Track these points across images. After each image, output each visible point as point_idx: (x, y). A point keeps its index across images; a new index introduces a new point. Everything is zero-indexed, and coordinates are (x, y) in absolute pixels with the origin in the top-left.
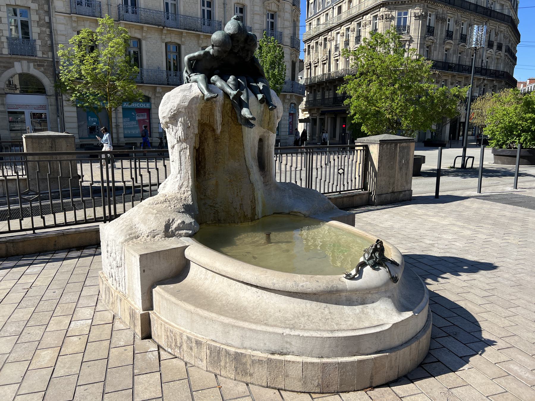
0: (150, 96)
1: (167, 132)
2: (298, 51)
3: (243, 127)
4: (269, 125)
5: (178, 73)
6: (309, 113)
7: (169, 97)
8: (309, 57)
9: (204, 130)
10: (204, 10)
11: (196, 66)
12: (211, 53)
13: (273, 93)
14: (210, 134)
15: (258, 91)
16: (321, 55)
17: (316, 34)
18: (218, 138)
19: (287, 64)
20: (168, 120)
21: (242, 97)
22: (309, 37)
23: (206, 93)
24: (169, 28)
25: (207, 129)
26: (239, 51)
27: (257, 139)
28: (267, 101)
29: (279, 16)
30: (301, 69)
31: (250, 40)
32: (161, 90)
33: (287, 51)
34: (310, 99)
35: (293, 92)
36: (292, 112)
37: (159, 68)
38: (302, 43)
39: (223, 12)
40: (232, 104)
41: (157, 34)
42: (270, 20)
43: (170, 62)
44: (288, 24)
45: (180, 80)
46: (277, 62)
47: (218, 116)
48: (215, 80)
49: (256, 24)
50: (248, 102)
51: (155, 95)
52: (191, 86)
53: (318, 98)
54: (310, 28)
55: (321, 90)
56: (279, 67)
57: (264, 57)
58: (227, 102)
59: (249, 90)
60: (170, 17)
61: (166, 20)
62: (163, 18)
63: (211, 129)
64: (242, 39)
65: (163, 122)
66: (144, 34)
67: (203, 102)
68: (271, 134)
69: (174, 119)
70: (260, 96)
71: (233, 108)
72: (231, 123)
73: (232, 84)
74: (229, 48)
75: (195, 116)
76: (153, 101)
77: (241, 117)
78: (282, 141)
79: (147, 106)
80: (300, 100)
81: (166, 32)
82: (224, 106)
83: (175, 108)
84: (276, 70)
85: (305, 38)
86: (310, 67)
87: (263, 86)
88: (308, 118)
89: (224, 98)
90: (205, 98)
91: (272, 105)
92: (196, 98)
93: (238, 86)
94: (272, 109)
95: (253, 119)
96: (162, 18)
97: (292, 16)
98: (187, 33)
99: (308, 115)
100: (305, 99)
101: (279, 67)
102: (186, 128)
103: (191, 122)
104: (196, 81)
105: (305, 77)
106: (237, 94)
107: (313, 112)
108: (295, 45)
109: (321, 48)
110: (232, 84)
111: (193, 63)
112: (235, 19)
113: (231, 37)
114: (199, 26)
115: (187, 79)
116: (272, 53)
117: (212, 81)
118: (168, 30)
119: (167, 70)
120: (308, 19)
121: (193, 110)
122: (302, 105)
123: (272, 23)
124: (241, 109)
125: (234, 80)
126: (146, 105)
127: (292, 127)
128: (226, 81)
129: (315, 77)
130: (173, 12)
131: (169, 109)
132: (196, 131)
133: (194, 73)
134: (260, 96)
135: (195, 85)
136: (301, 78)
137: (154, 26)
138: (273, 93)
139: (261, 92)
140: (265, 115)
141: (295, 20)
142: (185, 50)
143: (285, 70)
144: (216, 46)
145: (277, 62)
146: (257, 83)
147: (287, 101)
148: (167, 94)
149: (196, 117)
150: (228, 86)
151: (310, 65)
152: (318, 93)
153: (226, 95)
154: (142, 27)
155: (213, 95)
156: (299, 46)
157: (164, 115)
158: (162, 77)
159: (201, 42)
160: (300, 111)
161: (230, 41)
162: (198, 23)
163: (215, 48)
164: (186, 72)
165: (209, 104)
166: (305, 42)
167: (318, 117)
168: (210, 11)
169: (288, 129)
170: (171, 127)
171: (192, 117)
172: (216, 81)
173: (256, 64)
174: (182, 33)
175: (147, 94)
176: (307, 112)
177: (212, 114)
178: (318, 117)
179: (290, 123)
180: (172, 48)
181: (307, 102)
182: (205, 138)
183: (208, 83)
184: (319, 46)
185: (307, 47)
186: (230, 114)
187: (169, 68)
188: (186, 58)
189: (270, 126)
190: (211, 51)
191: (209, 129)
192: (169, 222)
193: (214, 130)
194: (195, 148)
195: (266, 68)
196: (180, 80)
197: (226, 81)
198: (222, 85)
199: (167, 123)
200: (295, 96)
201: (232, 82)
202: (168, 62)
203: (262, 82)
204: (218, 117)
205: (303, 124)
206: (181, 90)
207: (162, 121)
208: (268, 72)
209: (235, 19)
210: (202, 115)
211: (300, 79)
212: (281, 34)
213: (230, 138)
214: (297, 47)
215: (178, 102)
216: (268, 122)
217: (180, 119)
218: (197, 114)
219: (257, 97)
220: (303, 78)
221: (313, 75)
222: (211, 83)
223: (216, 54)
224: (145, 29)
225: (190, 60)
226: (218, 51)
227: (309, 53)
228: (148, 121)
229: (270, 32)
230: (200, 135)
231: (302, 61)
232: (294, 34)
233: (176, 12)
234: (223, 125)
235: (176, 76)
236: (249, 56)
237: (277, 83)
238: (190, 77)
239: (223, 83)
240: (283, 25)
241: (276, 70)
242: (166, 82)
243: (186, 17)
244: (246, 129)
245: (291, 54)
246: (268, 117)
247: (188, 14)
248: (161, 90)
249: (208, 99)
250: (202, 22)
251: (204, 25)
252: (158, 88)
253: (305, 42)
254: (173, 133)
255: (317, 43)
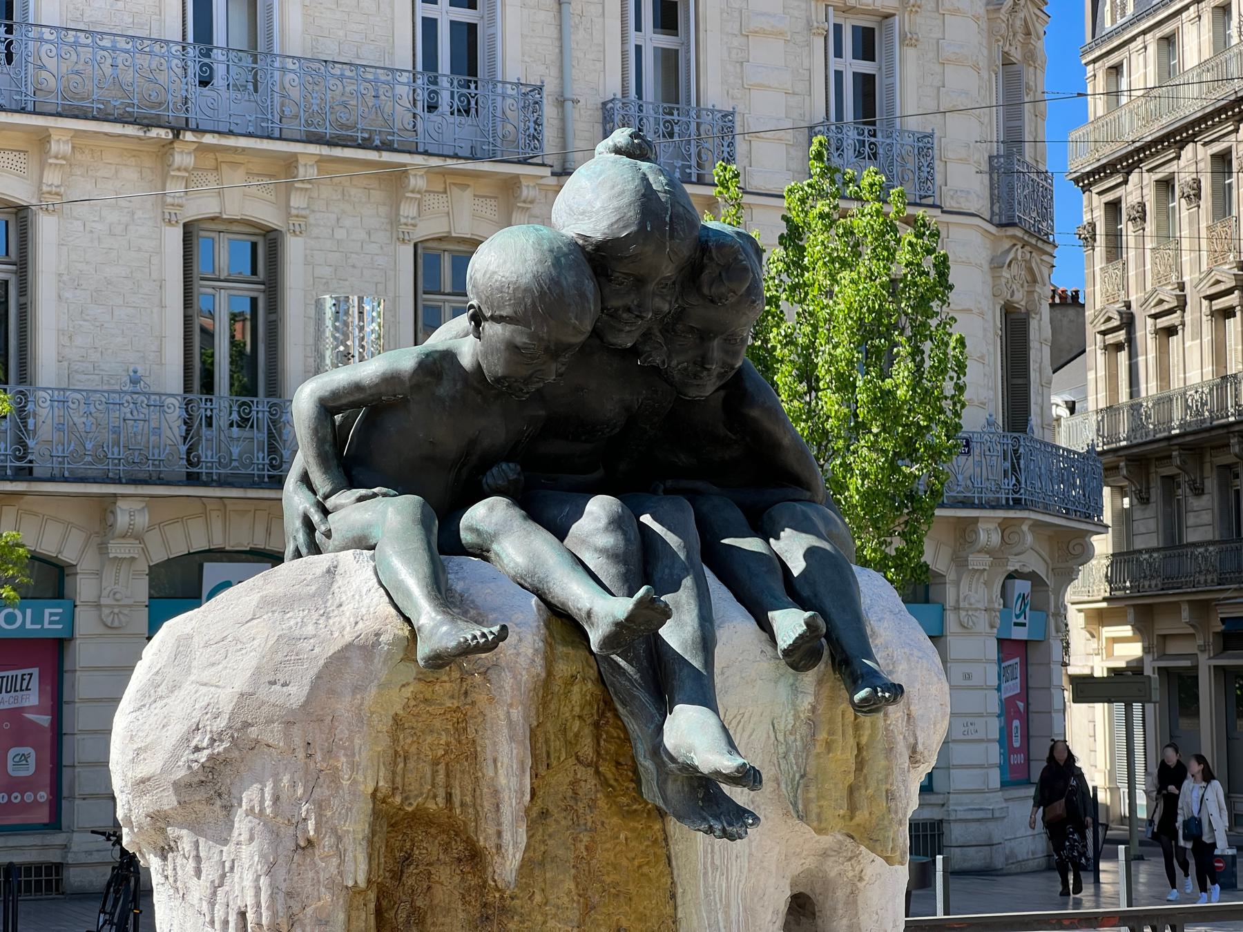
0: (68, 556)
1: (156, 879)
2: (1039, 239)
3: (675, 827)
4: (853, 809)
5: (260, 407)
6: (1143, 629)
7: (182, 649)
8: (1115, 270)
9: (408, 859)
10: (430, 26)
11: (363, 443)
12: (466, 360)
13: (876, 593)
14: (447, 882)
15: (779, 587)
16: (1198, 260)
17: (1151, 132)
18: (503, 910)
19: (971, 318)
20: (169, 801)
21: (664, 632)
22: (1108, 152)
23: (426, 614)
24: (209, 139)
25: (429, 848)
26: (647, 335)
27: (779, 899)
28: (836, 651)
29: (908, 40)
30: (1069, 352)
31: (717, 269)
32: (142, 520)
33: (969, 248)
34: (1139, 544)
35: (1018, 504)
36: (1019, 634)
37: (135, 381)
38: (1063, 190)
39: (552, 31)
40: (601, 680)
41: (130, 174)
42: (851, 66)
43: (208, 334)
44: (972, 84)
45: (273, 450)
46: (905, 314)
47: (504, 760)
48: (485, 527)
49: (759, 195)
50: (709, 661)
51: (103, 549)
52: (331, 572)
53: (1191, 537)
54: (1114, 94)
55: (1211, 484)
56: (916, 352)
57: (806, 338)
58: (563, 669)
59: (708, 572)
60: (220, 70)
61: (196, 91)
62: (171, 79)
63: (458, 848)
64: (668, 270)
65: (138, 815)
66: (52, 178)
67: (408, 673)
68: (873, 865)
69: (209, 787)
70: (790, 623)
71: (608, 703)
72: (592, 805)
73: (603, 551)
74: (579, 327)
75: (354, 767)
76: (84, 588)
77: (660, 766)
78: (955, 833)
79: (49, 620)
80: (1071, 553)
81: (189, 161)
82: (545, 692)
83: (222, 723)
84: (901, 373)
85: (1084, 162)
86: (1131, 340)
87: (810, 554)
88: (1135, 669)
89: (549, 643)
90: (423, 650)
91: (872, 677)
92: (365, 649)
93: (642, 564)
94: (869, 707)
95: (748, 777)
96: (171, 79)
97: (991, 32)
98: (322, 160)
99: (1135, 650)
100: (1103, 545)
101: (916, 352)
102: (293, 848)
103: (320, 807)
104: (363, 543)
105: (1096, 398)
106: (631, 617)
107: (1165, 626)
108: (1019, 206)
109: (1191, 221)
110: (603, 551)
111: (346, 424)
112: (618, 151)
113: (598, 259)
114: (402, 116)
115: (309, 526)
116: (865, 263)
117: (466, 537)
118: (202, 149)
119: (187, 388)
120: (1097, 39)
121: (342, 731)
122: (1090, 584)
123: (866, 84)
124: (664, 707)
125: (617, 523)
126: (37, 619)
127: (1026, 736)
128: (560, 533)
129: (1164, 401)
130: (239, 39)
131: (177, 730)
132: (357, 870)
133: (352, 485)
134: (790, 623)
135: (356, 571)
136: (1072, 408)
137: (117, 129)
138: (876, 593)
139: (795, 592)
140: (829, 746)
141: (1016, 55)
142: (308, 262)
143: (961, 367)
144: (494, 318)
145: (905, 314)
146: (767, 532)
147: (978, 561)
148: (166, 624)
149: (361, 774)
150: (570, 561)
151: (1128, 322)
152: (1195, 503)
153: (563, 623)
154: (42, 139)
155: (470, 632)
156: (1046, 214)
157: (143, 771)
158: (157, 431)
159: (408, 210)
160: (1076, 620)
161: (589, 286)
162: (395, 99)
163: (489, 328)
164: (305, 480)
165: (447, 683)
166: (1086, 181)
167: (1205, 665)
168: (472, 28)
169: (995, 749)
170: (186, 845)
171: (335, 778)
172: (494, 537)
173: (755, 413)
174: (291, 162)
175: (48, 547)
176: (1126, 631)
177: (465, 754)
178: (1205, 665)
179: (1009, 709)
180: (226, 256)
181: (1117, 558)
182: (414, 910)
183: (445, 543)
184: (1183, 209)
185: (1099, 215)
186: (586, 748)
187: (200, 377)
188: (304, 399)
189: (862, 816)
190: (468, 351)
191: (446, 848)
192: (241, 353)
193: (474, 857)
194: (381, 394)
195: (833, 360)
196: (273, 450)
197: (560, 533)
198: (534, 557)
199: (159, 820)
200: (1037, 525)
201: (608, 540)
202: (196, 337)
203: (803, 526)
204: (507, 771)
205: (1100, 709)
206: (267, 604)
207: (129, 807)
208: (845, 385)
209: (618, 151)
210: (397, 757)
211: (1063, 412)
212: (925, 145)
213: (588, 908)
214: (1030, 218)
215: (240, 682)
216: (851, 790)
217: (250, 796)
218: (364, 757)
219: (765, 626)
220: (1080, 410)
221: (1149, 387)
222: (461, 550)
223: (495, 367)
224: (59, 146)
225: (327, 407)
226: (512, 348)
227: (1115, 249)
228: (45, 720)
229: (851, 135)
230: (382, 893)
231: (1071, 302)
232: (1013, 140)
233: (257, 41)
234: (538, 817)
235: (244, 422)
236: (715, 368)
237: (908, 450)
238: (326, 512)
239: (541, 540)
240: (941, 88)
241: (901, 373)
242: (181, 468)
243: (317, 67)
244: (695, 846)
245: (996, 265)
246: (845, 755)
247: (330, 52)
248: (142, 520)
249: (438, 661)
250: (421, 96)
251: (432, 108)
252: (122, 504)
253: (1086, 181)
254: (198, 890)
255: (1166, 185)
